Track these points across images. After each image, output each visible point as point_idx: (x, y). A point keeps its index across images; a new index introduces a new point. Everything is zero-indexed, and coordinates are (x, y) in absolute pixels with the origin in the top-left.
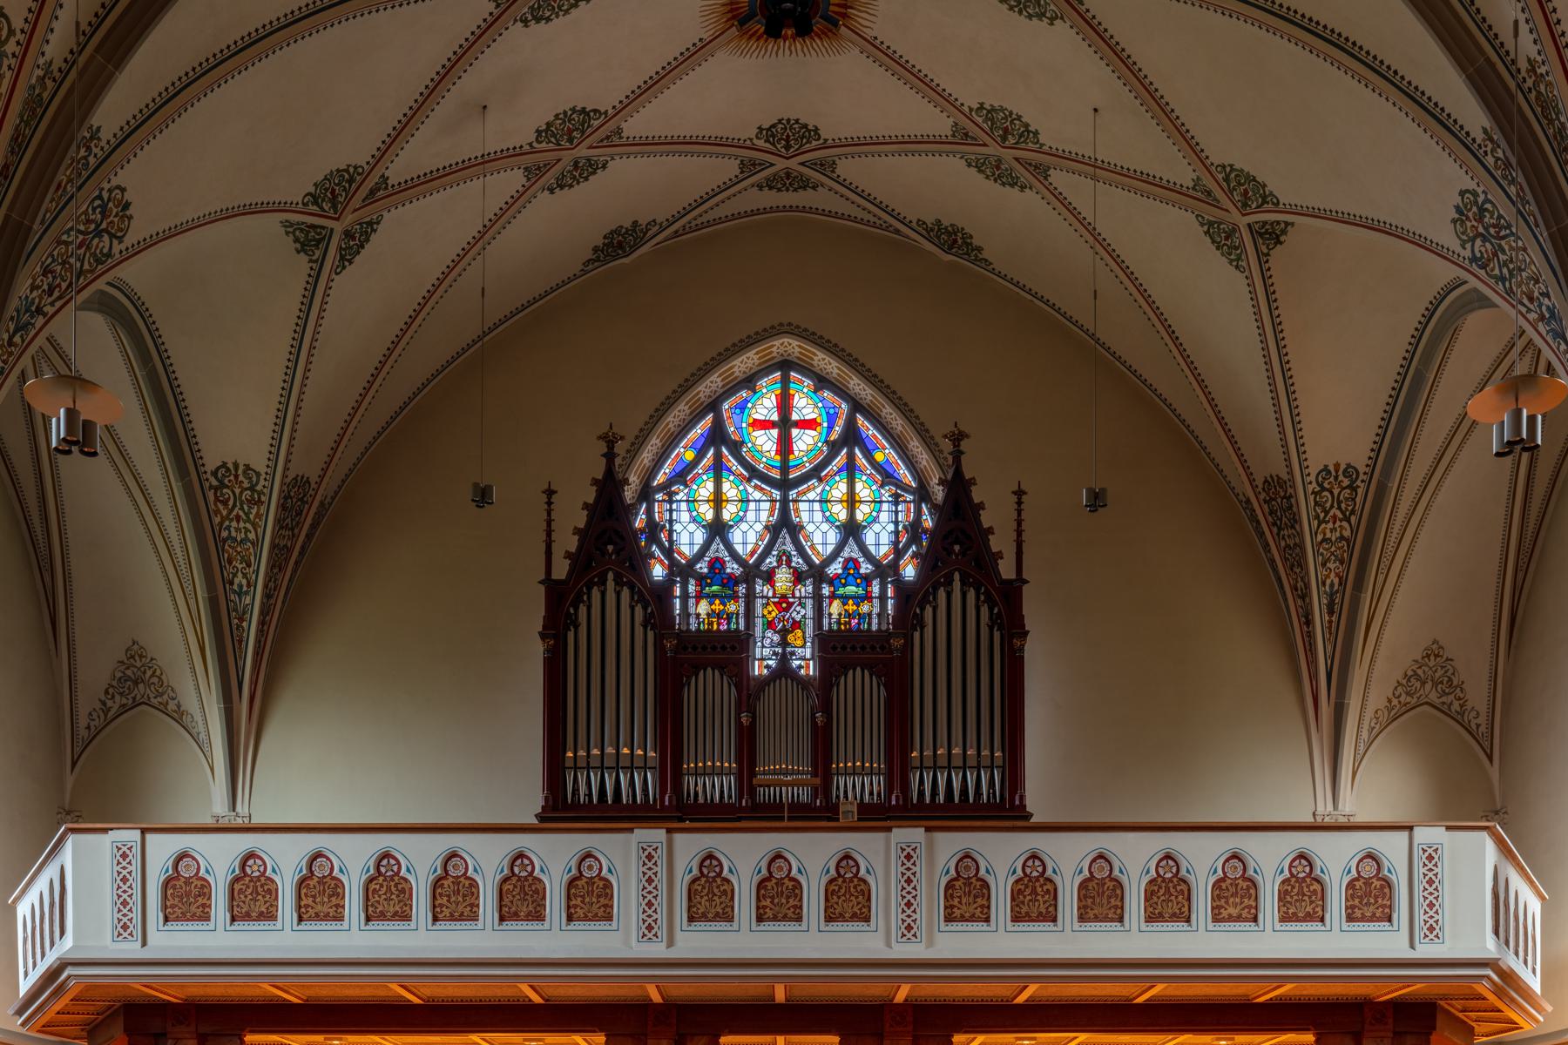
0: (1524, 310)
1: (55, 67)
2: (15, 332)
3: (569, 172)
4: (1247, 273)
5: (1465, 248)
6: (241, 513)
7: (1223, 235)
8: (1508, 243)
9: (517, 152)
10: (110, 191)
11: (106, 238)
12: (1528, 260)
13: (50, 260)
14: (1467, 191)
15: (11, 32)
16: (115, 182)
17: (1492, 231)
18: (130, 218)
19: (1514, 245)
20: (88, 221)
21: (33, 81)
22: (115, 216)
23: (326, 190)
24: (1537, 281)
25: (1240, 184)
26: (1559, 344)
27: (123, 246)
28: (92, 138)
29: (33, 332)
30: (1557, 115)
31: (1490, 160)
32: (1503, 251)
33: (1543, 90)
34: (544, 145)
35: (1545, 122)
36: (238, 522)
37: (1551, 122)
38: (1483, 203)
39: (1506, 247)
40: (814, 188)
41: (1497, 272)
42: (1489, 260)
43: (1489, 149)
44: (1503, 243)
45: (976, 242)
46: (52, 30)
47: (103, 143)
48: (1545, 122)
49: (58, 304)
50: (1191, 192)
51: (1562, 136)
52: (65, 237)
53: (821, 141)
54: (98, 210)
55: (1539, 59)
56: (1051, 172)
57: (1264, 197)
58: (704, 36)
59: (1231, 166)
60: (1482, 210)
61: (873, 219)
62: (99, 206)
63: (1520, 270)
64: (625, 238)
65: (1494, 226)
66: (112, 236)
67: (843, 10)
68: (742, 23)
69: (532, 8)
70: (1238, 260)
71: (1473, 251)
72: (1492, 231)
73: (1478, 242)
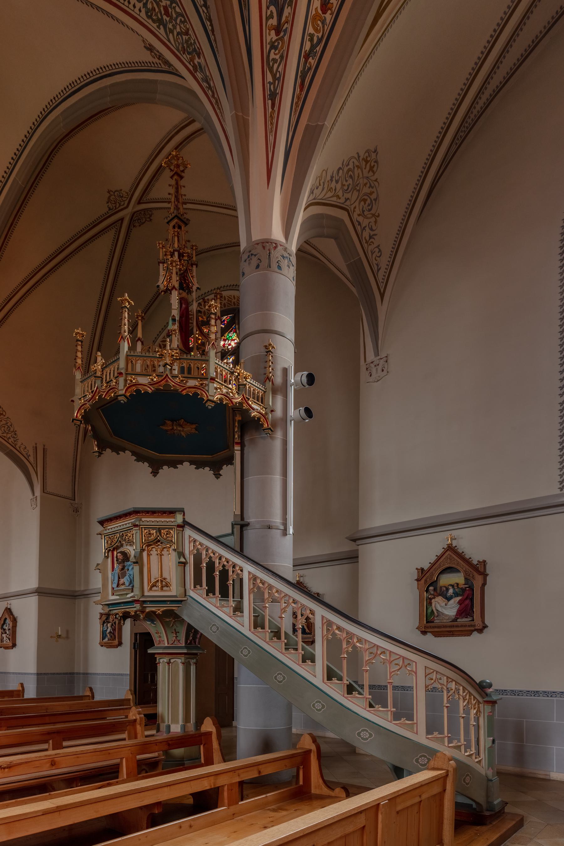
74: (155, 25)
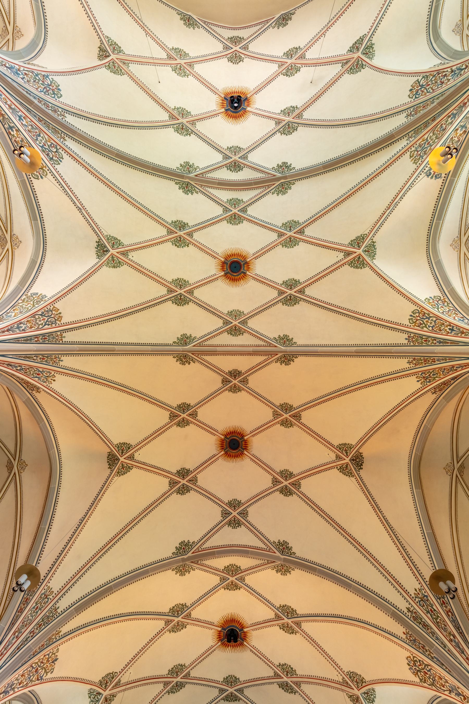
0: (26, 69)
1: (407, 138)
2: (462, 69)
3: (294, 54)
4: (104, 36)
5: (52, 78)
6: (426, 320)
7: (116, 49)
8: (42, 87)
9: (307, 65)
10: (412, 98)
11: (421, 83)
12: (34, 86)
13: (439, 86)
14: (60, 97)
15: (411, 152)
16: (410, 100)
17: (48, 89)
18: (412, 86)
19: (40, 88)
20: (423, 91)
21: (413, 138)
22: (415, 89)
23: (358, 68)
24: (28, 81)
25: (117, 70)
26: (9, 65)
27: (418, 78)
28: (409, 115)
29: (458, 66)
30: (52, 131)
31: (60, 110)
32: (42, 84)
33: (59, 135)
34: (299, 66)
35: (54, 127)
36: (428, 322)
37: (52, 128)
38: (55, 96)
39: (42, 86)
40: (229, 38)
41: (39, 76)
42: (44, 79)
43: (62, 113)
44: (43, 87)
45: (182, 22)
46: (402, 148)
47: (407, 113)
48: (54, 127)
49: (446, 70)
50: (128, 62)
51: (48, 126)
52: (431, 91)
53: (227, 57)
54: (418, 94)
55: (64, 142)
56: (166, 57)
57: (110, 68)
58: (255, 95)
59: (121, 75)
60: (54, 94)
61: (212, 27)
62: (417, 95)
63: (35, 81)
64: (282, 22)
65: (48, 90)
66: (419, 83)
67: (223, 102)
68: (247, 98)
69: (294, 111)
70: (109, 40)
71: (49, 79)
72: (48, 89)
73: (49, 83)
74: (431, 687)
